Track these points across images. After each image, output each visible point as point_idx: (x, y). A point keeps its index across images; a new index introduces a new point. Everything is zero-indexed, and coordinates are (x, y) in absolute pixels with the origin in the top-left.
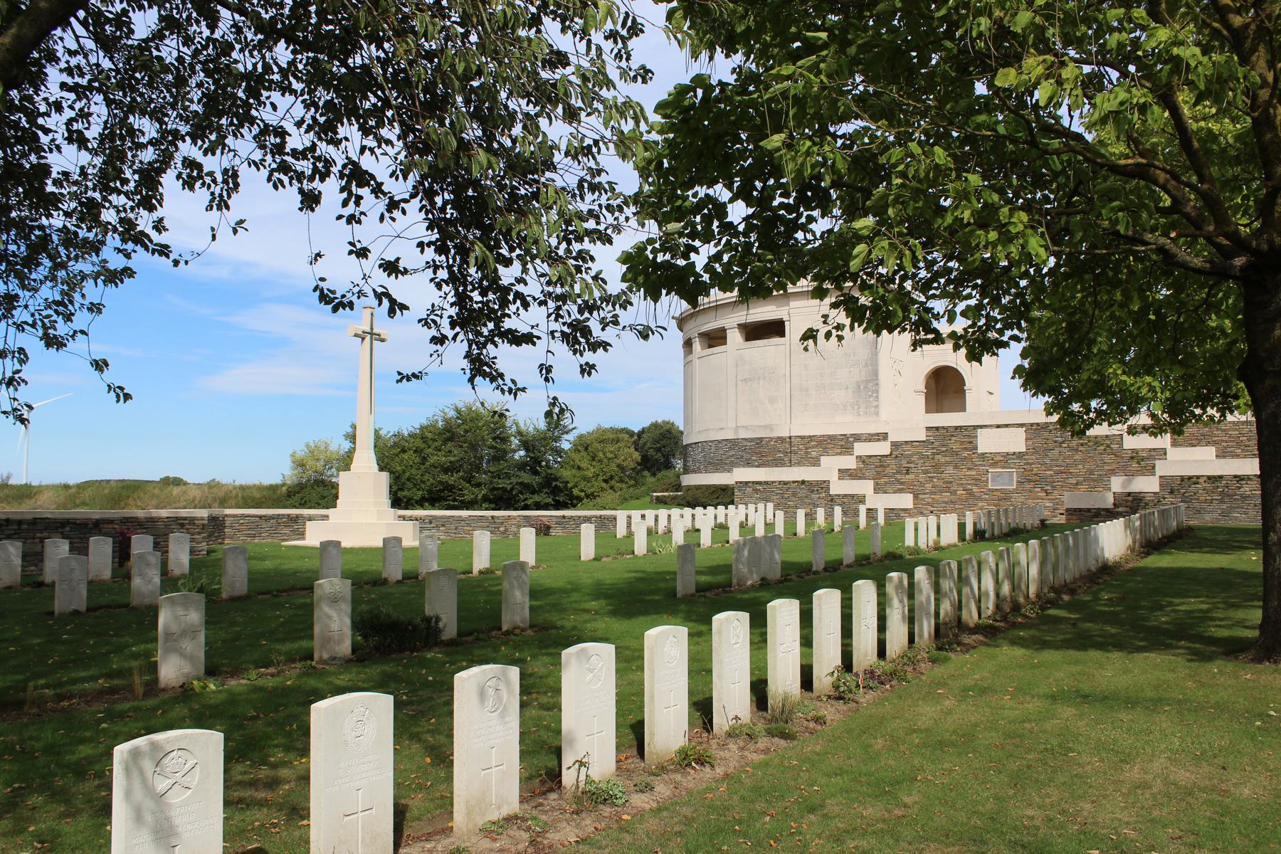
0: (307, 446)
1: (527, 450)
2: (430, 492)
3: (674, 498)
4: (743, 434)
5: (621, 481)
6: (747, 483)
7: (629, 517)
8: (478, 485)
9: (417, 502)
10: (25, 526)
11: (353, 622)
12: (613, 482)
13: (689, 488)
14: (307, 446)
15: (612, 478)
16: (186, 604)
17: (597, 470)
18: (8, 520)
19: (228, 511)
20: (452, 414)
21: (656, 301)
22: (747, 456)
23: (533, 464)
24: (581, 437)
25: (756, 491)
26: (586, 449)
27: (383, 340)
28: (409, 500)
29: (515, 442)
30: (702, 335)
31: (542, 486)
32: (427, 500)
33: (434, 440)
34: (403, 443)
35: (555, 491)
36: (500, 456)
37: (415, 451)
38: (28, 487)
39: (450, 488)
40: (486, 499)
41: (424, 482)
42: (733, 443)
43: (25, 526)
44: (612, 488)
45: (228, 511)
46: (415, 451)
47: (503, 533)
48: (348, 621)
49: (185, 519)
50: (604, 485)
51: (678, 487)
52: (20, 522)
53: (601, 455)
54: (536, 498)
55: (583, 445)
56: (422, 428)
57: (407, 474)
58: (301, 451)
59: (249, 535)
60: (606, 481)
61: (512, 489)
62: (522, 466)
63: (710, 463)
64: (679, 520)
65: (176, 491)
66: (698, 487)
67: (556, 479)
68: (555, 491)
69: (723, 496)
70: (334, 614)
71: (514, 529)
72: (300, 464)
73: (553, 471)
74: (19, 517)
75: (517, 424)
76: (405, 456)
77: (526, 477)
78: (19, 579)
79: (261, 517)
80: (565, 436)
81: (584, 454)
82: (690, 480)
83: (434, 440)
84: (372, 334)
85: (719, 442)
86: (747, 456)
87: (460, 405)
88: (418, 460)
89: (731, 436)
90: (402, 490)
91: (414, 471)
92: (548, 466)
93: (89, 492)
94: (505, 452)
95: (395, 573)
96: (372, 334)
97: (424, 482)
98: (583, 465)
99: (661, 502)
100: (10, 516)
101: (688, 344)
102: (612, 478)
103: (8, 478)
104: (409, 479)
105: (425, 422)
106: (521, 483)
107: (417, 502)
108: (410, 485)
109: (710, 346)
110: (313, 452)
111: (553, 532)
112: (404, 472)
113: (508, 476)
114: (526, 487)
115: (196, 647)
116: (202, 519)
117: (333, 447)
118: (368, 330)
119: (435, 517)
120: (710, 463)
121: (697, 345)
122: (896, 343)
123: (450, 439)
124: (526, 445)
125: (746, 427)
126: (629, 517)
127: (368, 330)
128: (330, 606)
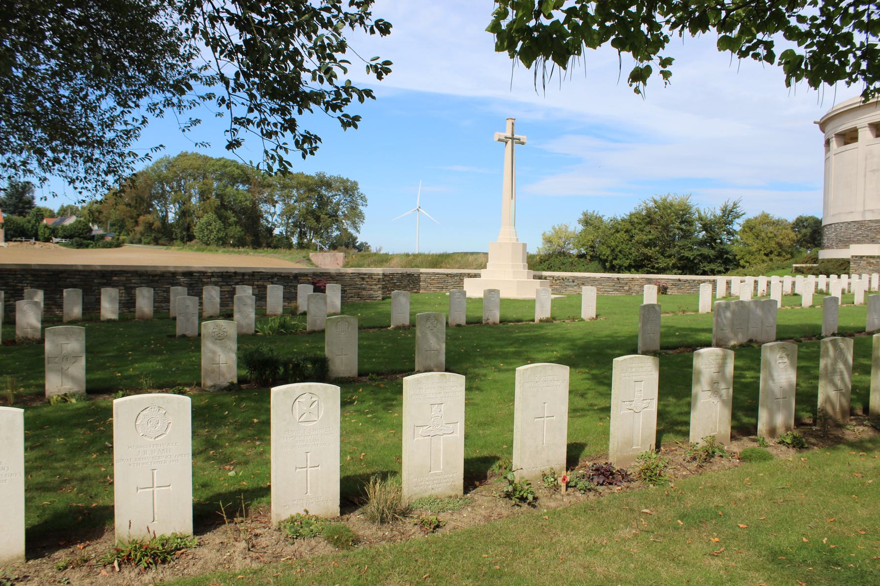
0: (554, 228)
1: (706, 230)
2: (635, 261)
3: (810, 268)
4: (869, 217)
5: (779, 255)
6: (862, 257)
7: (756, 282)
8: (669, 256)
9: (626, 268)
10: (247, 277)
11: (239, 358)
12: (772, 256)
13: (823, 261)
14: (554, 228)
15: (771, 252)
16: (67, 335)
17: (760, 246)
18: (235, 273)
19: (422, 270)
20: (651, 204)
21: (565, 68)
22: (871, 235)
23: (711, 241)
24: (748, 221)
25: (869, 264)
26: (751, 229)
27: (523, 143)
28: (620, 266)
29: (698, 225)
30: (838, 135)
31: (717, 258)
32: (633, 267)
33: (640, 224)
34: (617, 225)
35: (727, 262)
36: (687, 235)
37: (626, 232)
38: (387, 255)
39: (648, 258)
40: (674, 266)
41: (631, 254)
42: (860, 224)
43: (247, 277)
44: (771, 260)
45: (422, 270)
46: (626, 232)
47: (628, 291)
48: (234, 357)
49: (365, 274)
50: (765, 258)
51: (815, 260)
52: (243, 274)
53: (763, 234)
54: (712, 266)
55: (749, 227)
56: (631, 215)
57: (619, 248)
58: (549, 231)
59: (438, 288)
60: (766, 255)
61: (694, 259)
62: (702, 243)
63: (840, 241)
64: (807, 286)
65: (471, 258)
66: (829, 261)
67: (727, 253)
68: (727, 262)
69: (842, 267)
70: (218, 350)
71: (637, 288)
72: (549, 241)
73: (726, 247)
74: (243, 271)
75: (699, 213)
76: (618, 235)
77: (705, 251)
78: (218, 311)
79: (447, 275)
80: (737, 220)
81: (750, 234)
82: (825, 254)
83: (640, 224)
84: (512, 139)
85: (849, 223)
86: (871, 235)
87: (657, 198)
88: (627, 237)
89: (858, 218)
90: (615, 259)
91: (624, 246)
92: (721, 243)
93: (419, 260)
94: (692, 234)
95: (495, 316)
96: (512, 139)
97: (631, 254)
98: (750, 242)
99: (799, 271)
100: (238, 271)
101: (828, 143)
102: (771, 252)
103: (380, 250)
104: (620, 252)
105: (634, 211)
106: (701, 255)
107: (626, 268)
108: (621, 256)
109: (846, 143)
110: (558, 233)
111: (669, 292)
112: (617, 246)
113: (691, 249)
114: (705, 258)
115: (79, 369)
116: (378, 275)
117: (571, 229)
118: (510, 135)
119: (577, 278)
120: (840, 241)
121: (834, 144)
122: (628, 55)
123: (650, 223)
124: (705, 227)
125: (872, 211)
126: (756, 282)
127: (510, 135)
128: (214, 343)
